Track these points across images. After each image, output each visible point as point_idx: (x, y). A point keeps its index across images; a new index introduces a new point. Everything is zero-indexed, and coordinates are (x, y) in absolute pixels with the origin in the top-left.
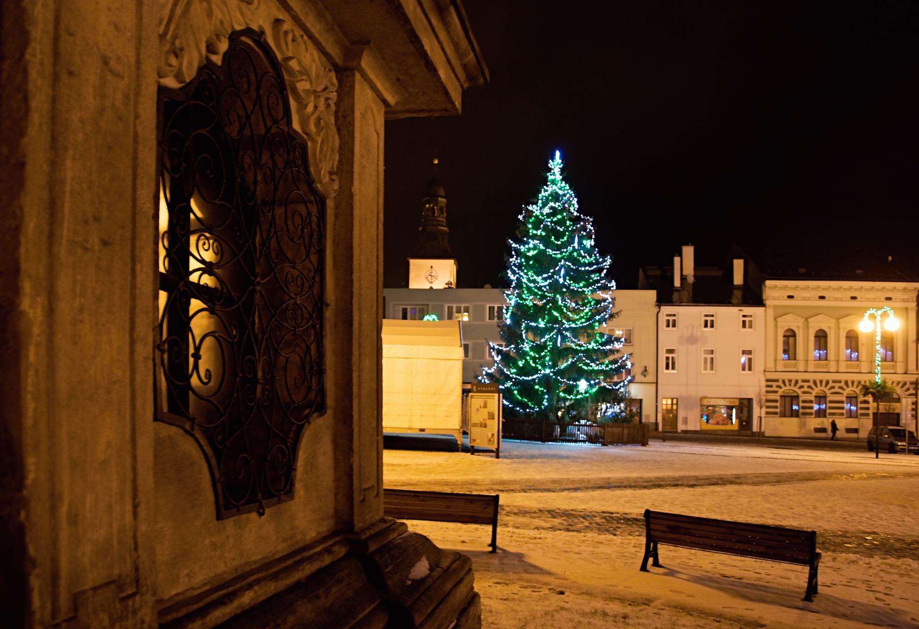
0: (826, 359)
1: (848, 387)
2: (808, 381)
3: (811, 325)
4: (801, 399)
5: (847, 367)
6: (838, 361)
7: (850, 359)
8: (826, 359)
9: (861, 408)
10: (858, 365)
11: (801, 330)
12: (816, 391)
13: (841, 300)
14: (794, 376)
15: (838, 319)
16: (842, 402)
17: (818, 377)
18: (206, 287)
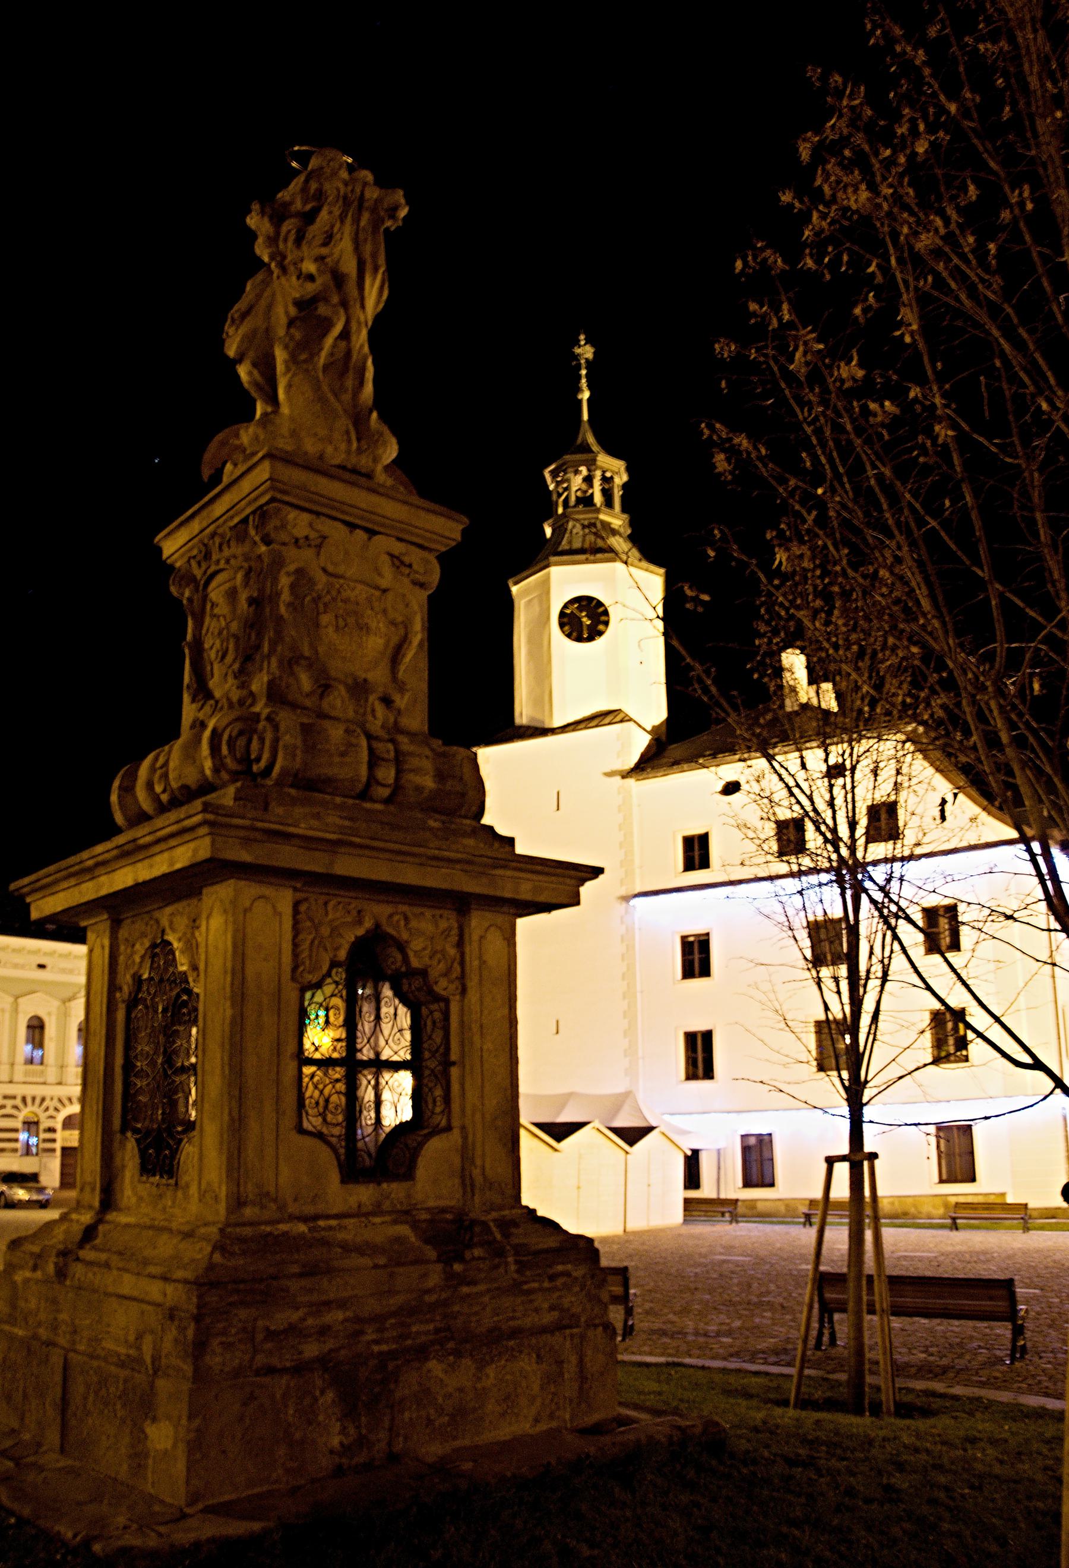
0: (42, 1063)
1: (64, 1105)
2: (14, 1097)
3: (21, 1008)
4: (42, 1127)
5: (26, 1074)
6: (12, 1064)
7: (30, 1061)
8: (42, 1063)
9: (45, 1141)
10: (42, 1072)
11: (54, 1018)
12: (24, 1113)
13: (22, 967)
14: (39, 1091)
15: (17, 998)
16: (16, 1130)
17: (29, 1091)
18: (392, 988)
